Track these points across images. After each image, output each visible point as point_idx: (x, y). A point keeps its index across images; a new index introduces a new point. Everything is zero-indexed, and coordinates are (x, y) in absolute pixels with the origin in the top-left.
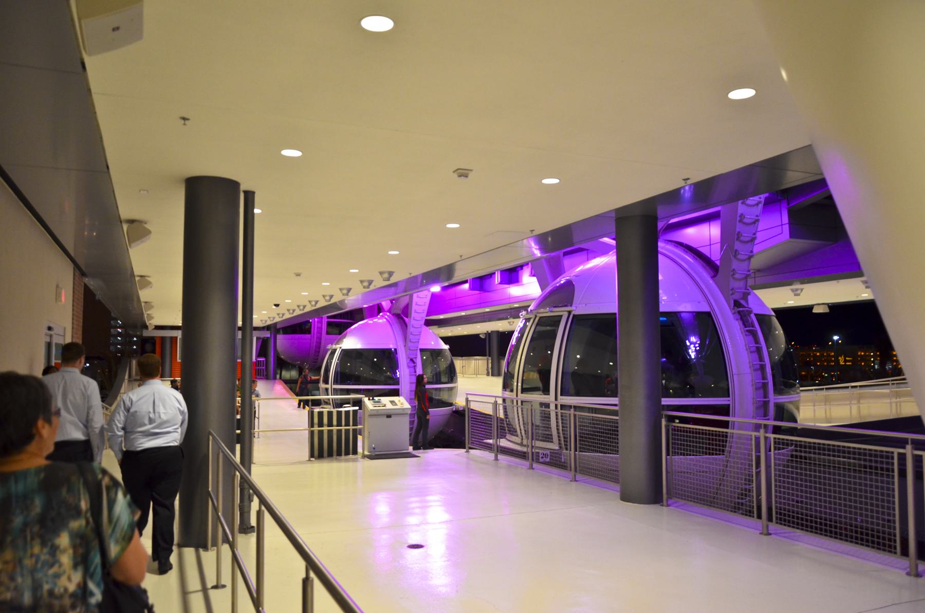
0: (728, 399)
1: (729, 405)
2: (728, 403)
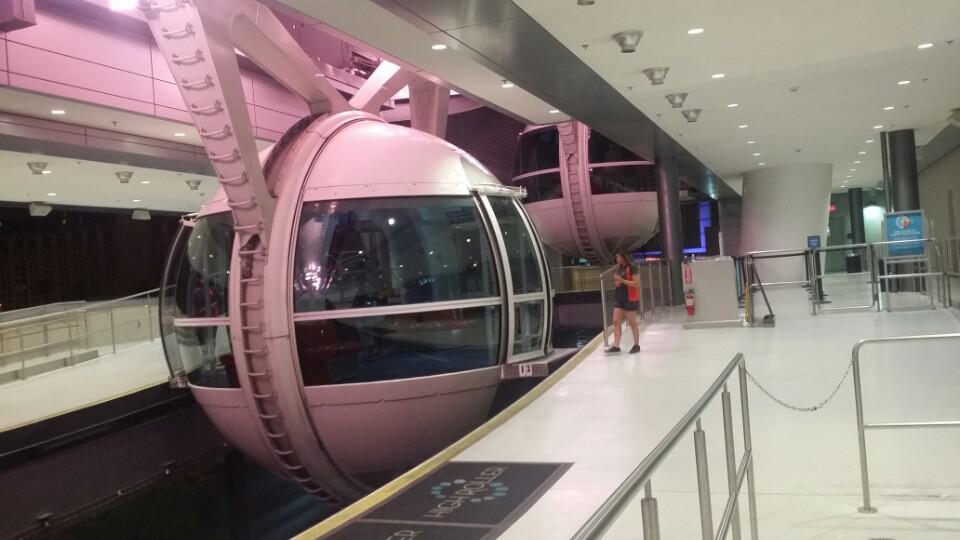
0: (296, 320)
1: (295, 311)
2: (296, 314)
